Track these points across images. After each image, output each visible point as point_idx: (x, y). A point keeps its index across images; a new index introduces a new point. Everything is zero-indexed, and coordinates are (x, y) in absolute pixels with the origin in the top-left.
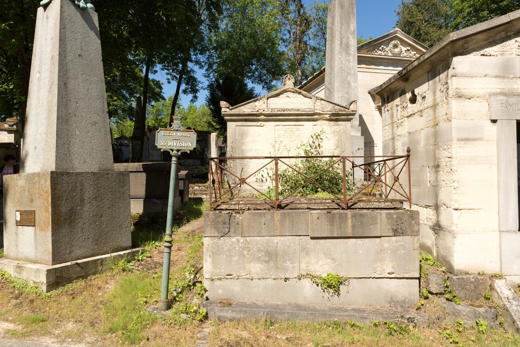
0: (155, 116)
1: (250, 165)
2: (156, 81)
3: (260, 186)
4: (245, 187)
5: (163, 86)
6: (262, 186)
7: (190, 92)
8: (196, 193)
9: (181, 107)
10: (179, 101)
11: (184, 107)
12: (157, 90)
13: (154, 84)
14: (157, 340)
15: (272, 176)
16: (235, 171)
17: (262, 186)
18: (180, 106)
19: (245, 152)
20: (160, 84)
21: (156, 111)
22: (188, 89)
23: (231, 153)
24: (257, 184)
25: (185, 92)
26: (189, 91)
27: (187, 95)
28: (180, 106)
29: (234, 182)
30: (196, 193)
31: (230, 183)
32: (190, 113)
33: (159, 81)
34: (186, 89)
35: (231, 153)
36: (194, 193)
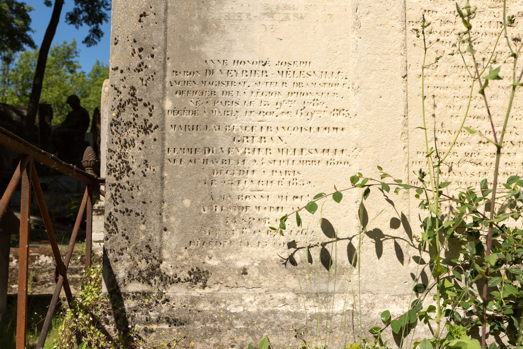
0: (21, 88)
1: (250, 157)
2: (17, 3)
3: (309, 296)
4: (214, 301)
5: (31, 14)
6: (328, 294)
7: (87, 20)
8: (41, 277)
9: (78, 71)
10: (73, 57)
11: (83, 69)
12: (18, 22)
13: (11, 8)
14: (182, 252)
15: (387, 230)
16: (155, 196)
17: (328, 294)
18: (75, 67)
19: (218, 76)
20: (25, 11)
21: (23, 77)
22: (80, 12)
23: (135, 79)
24: (292, 282)
25: (73, 18)
26: (84, 18)
27: (77, 28)
28: (75, 67)
29: (143, 265)
30: (41, 277)
31: (121, 273)
32: (96, 83)
33: (22, 4)
34: (77, 12)
35: (135, 79)
36: (35, 280)
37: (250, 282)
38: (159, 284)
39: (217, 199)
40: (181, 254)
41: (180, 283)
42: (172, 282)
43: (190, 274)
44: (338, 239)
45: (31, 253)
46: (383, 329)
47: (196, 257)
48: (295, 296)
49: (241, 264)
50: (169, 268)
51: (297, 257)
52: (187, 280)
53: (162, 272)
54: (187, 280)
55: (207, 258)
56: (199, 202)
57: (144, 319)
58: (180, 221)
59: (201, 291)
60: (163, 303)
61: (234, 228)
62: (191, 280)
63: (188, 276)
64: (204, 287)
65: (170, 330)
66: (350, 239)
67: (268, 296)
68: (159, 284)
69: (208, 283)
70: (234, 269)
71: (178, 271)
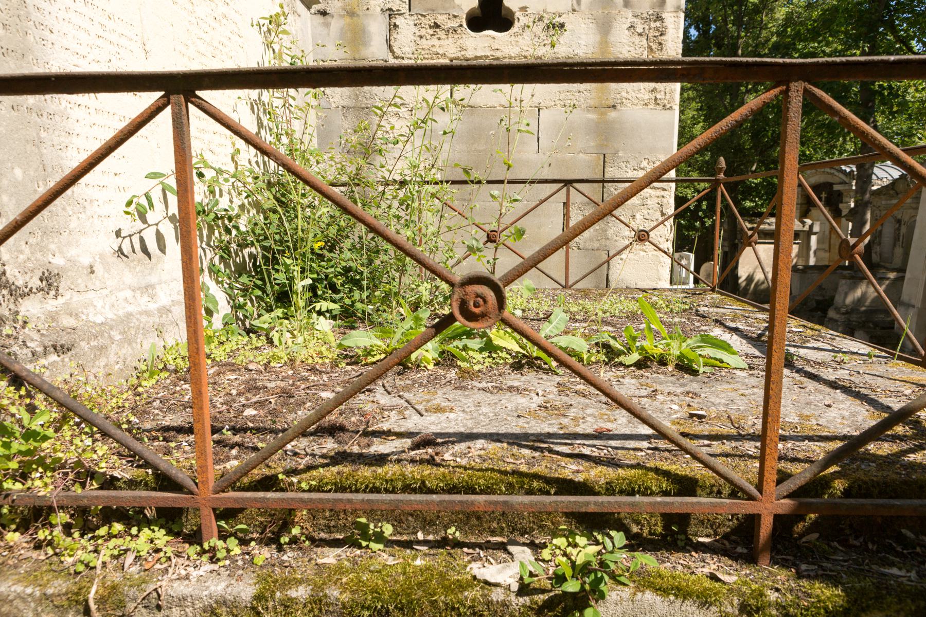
37: (97, 282)
38: (9, 300)
39: (50, 170)
40: (21, 252)
41: (32, 295)
42: (23, 296)
43: (41, 280)
44: (149, 226)
45: (899, 25)
46: (894, 245)
47: (39, 255)
48: (132, 293)
49: (86, 261)
50: (17, 274)
51: (126, 248)
52: (40, 290)
53: (11, 282)
54: (40, 290)
55: (51, 256)
56: (32, 173)
57: (30, 355)
58: (14, 201)
59: (55, 302)
60: (23, 327)
61: (71, 213)
62: (42, 290)
63: (39, 282)
64: (56, 297)
65: (63, 361)
66: (157, 225)
67: (113, 297)
68: (9, 300)
69: (61, 290)
70: (83, 268)
71: (27, 277)
